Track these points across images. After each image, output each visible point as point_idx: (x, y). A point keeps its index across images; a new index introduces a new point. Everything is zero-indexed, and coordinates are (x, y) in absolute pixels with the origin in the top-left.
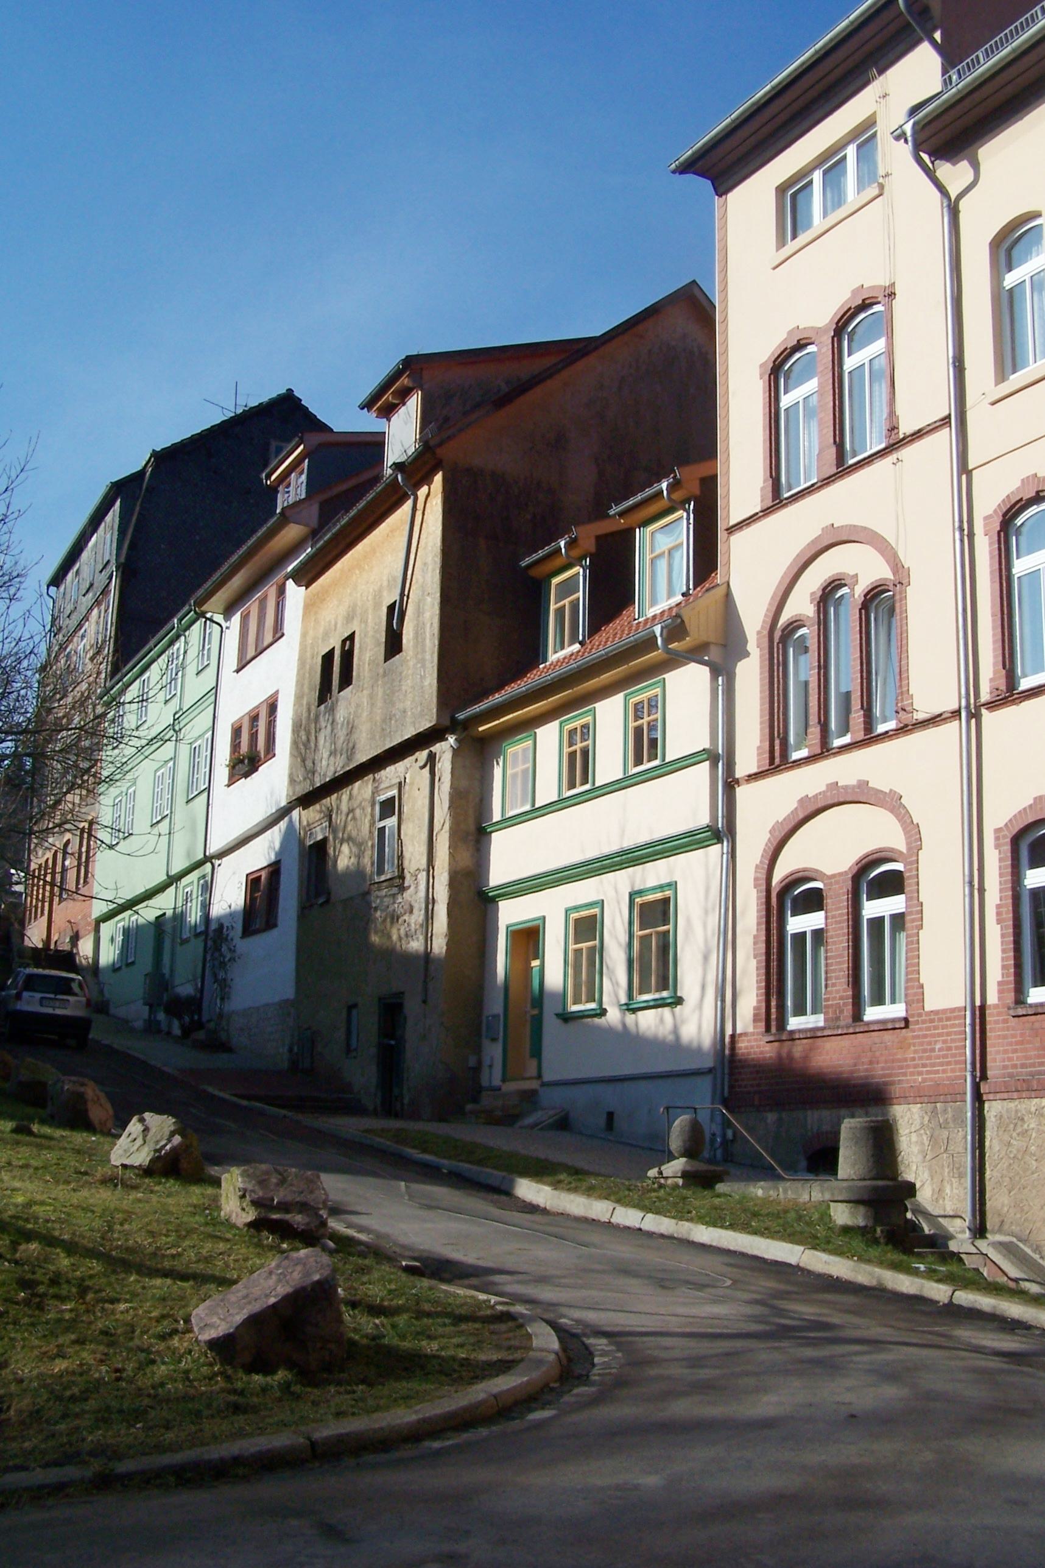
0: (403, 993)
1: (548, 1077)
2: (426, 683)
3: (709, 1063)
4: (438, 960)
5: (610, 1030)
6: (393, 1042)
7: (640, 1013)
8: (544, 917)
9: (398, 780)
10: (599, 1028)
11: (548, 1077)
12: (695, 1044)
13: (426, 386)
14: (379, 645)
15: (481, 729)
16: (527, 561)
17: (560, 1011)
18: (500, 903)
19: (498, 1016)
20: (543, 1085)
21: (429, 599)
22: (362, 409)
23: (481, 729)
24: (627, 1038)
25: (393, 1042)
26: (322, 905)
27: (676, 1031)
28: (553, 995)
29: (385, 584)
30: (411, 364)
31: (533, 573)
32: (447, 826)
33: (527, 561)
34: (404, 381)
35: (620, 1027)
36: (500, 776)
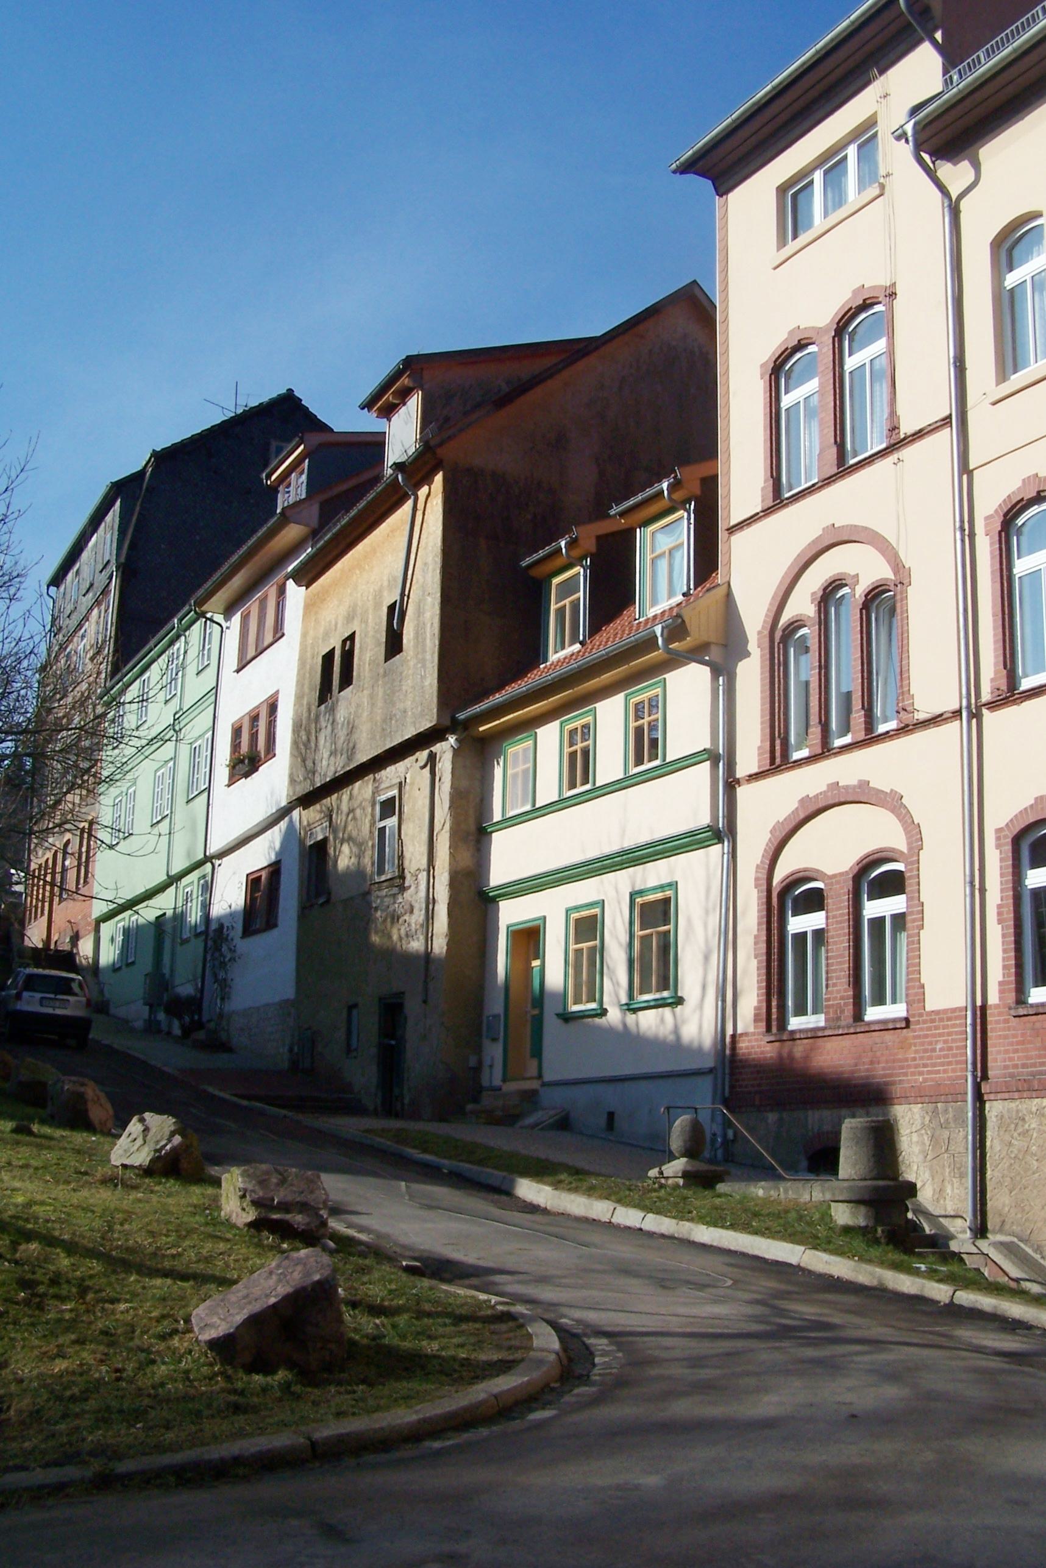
0: (403, 993)
1: (548, 1077)
2: (427, 683)
3: (710, 1063)
4: (439, 960)
5: (610, 1030)
6: (393, 1042)
7: (640, 1013)
8: (545, 917)
9: (398, 780)
10: (600, 1028)
11: (548, 1077)
12: (696, 1044)
13: (426, 386)
14: (379, 645)
15: (481, 729)
16: (528, 561)
17: (561, 1011)
18: (501, 903)
19: (499, 1016)
20: (544, 1085)
21: (429, 599)
22: (363, 409)
23: (481, 729)
24: (628, 1038)
25: (393, 1042)
26: (322, 905)
27: (676, 1031)
28: (554, 995)
29: (385, 584)
30: (411, 364)
31: (533, 573)
32: (447, 826)
33: (528, 561)
34: (405, 381)
35: (620, 1027)
36: (501, 776)
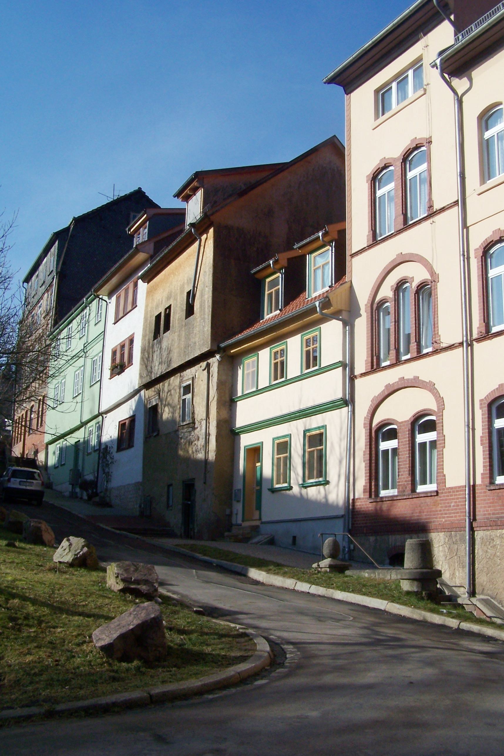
0: (194, 479)
1: (264, 519)
2: (206, 329)
3: (342, 513)
4: (211, 463)
5: (294, 497)
6: (189, 503)
7: (309, 489)
8: (262, 442)
9: (192, 376)
10: (289, 496)
11: (264, 519)
12: (335, 503)
13: (205, 186)
14: (183, 311)
15: (232, 351)
16: (254, 270)
17: (270, 487)
18: (241, 435)
19: (240, 490)
20: (262, 523)
21: (207, 289)
22: (175, 197)
23: (232, 351)
24: (302, 500)
25: (189, 503)
26: (155, 436)
27: (326, 497)
28: (267, 480)
30: (198, 176)
31: (257, 276)
32: (216, 398)
33: (254, 270)
34: (195, 183)
35: (299, 495)
36: (241, 374)
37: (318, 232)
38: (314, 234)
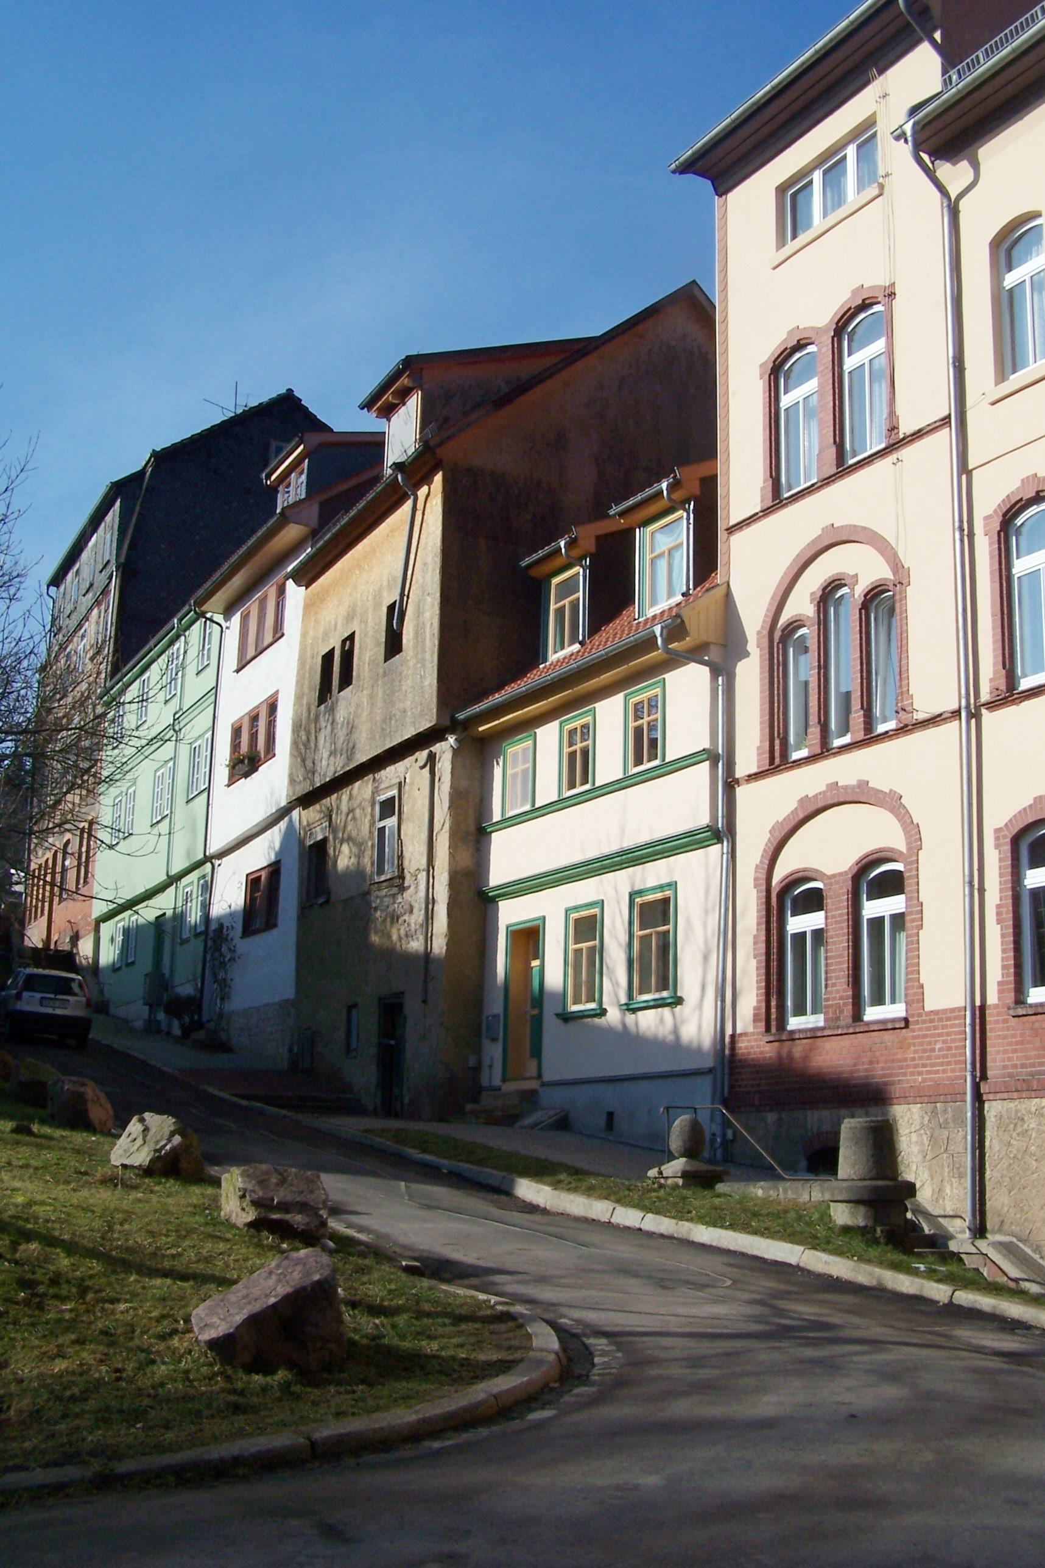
0: (403, 993)
1: (548, 1077)
2: (426, 683)
3: (709, 1063)
4: (438, 960)
5: (610, 1030)
6: (393, 1042)
7: (640, 1013)
8: (544, 917)
9: (398, 780)
10: (599, 1028)
11: (548, 1077)
12: (695, 1044)
13: (426, 386)
14: (379, 645)
15: (481, 729)
16: (527, 561)
17: (560, 1011)
19: (498, 1016)
20: (543, 1085)
21: (429, 599)
22: (362, 409)
23: (481, 729)
24: (627, 1038)
25: (393, 1042)
26: (322, 905)
27: (676, 1031)
28: (553, 995)
29: (385, 584)
30: (411, 364)
31: (533, 573)
32: (447, 826)
33: (527, 561)
34: (404, 381)
35: (620, 1027)
36: (500, 776)
37: (659, 481)
38: (650, 485)
